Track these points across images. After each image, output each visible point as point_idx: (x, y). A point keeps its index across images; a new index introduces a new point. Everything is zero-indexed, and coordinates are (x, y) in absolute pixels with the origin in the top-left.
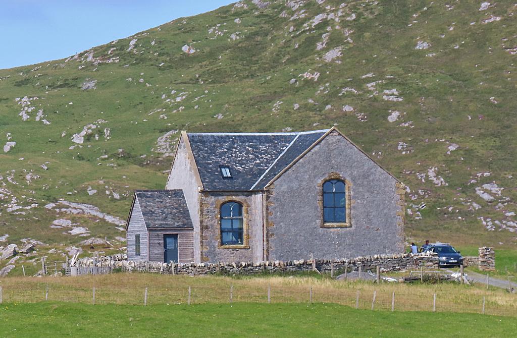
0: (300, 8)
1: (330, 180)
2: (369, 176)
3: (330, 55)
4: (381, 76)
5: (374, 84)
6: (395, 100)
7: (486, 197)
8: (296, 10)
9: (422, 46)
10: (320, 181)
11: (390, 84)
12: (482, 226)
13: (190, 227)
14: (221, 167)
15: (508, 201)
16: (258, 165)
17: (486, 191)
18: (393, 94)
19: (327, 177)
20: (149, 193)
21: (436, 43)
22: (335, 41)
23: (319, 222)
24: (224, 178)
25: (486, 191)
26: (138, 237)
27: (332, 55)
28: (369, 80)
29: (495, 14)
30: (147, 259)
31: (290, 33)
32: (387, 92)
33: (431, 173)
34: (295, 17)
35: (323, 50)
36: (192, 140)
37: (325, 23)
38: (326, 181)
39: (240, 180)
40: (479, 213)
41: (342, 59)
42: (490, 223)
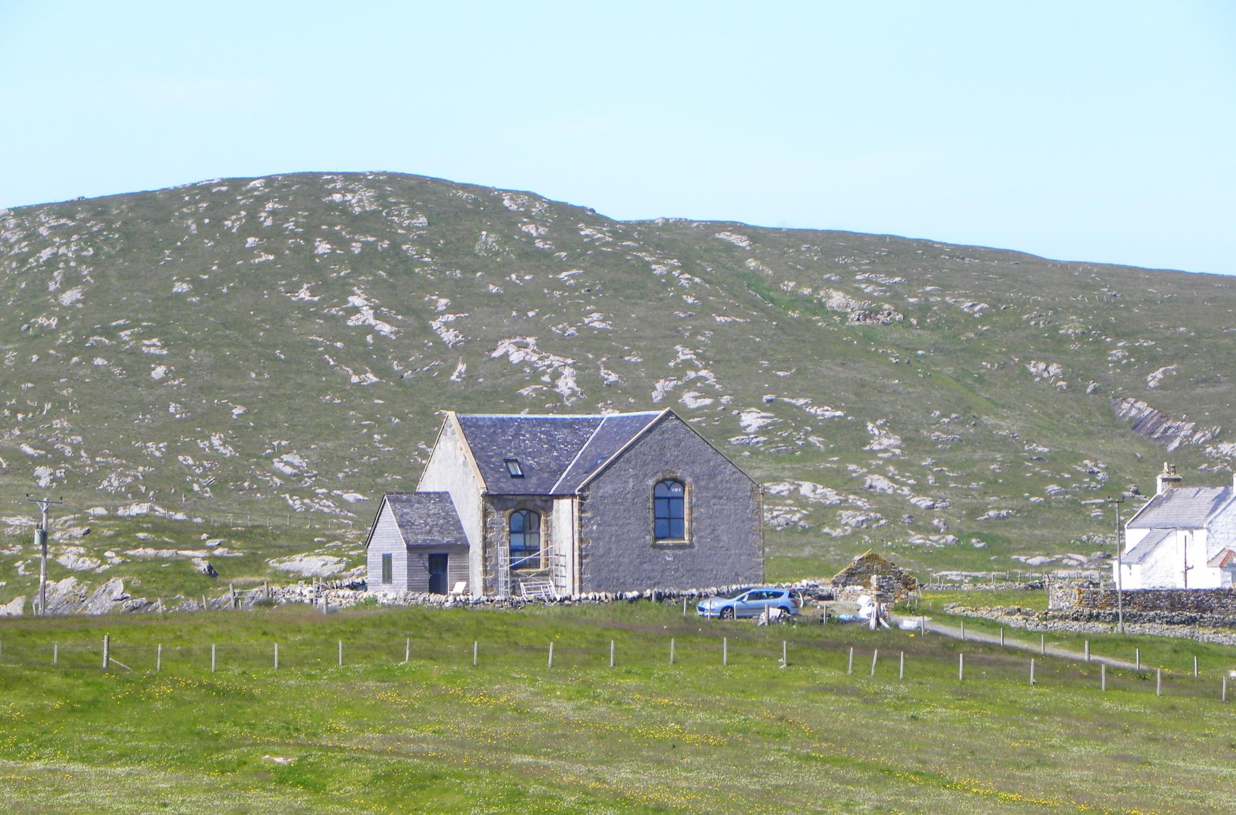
0: (18, 242)
1: (663, 481)
2: (715, 476)
3: (69, 297)
4: (136, 323)
5: (128, 332)
6: (158, 352)
7: (288, 470)
8: (16, 242)
9: (181, 287)
10: (651, 482)
11: (149, 333)
12: (288, 505)
13: (464, 548)
14: (507, 461)
15: (315, 476)
16: (557, 458)
17: (287, 463)
18: (154, 345)
19: (660, 476)
20: (405, 497)
21: (198, 286)
22: (71, 280)
23: (649, 538)
24: (513, 476)
25: (287, 463)
26: (387, 560)
27: (69, 297)
28: (124, 328)
29: (268, 252)
30: (404, 589)
31: (13, 270)
32: (146, 342)
33: (216, 441)
34: (16, 250)
35: (57, 289)
36: (464, 424)
37: (52, 263)
38: (658, 482)
39: (534, 480)
40: (281, 489)
41: (83, 302)
42: (298, 502)
